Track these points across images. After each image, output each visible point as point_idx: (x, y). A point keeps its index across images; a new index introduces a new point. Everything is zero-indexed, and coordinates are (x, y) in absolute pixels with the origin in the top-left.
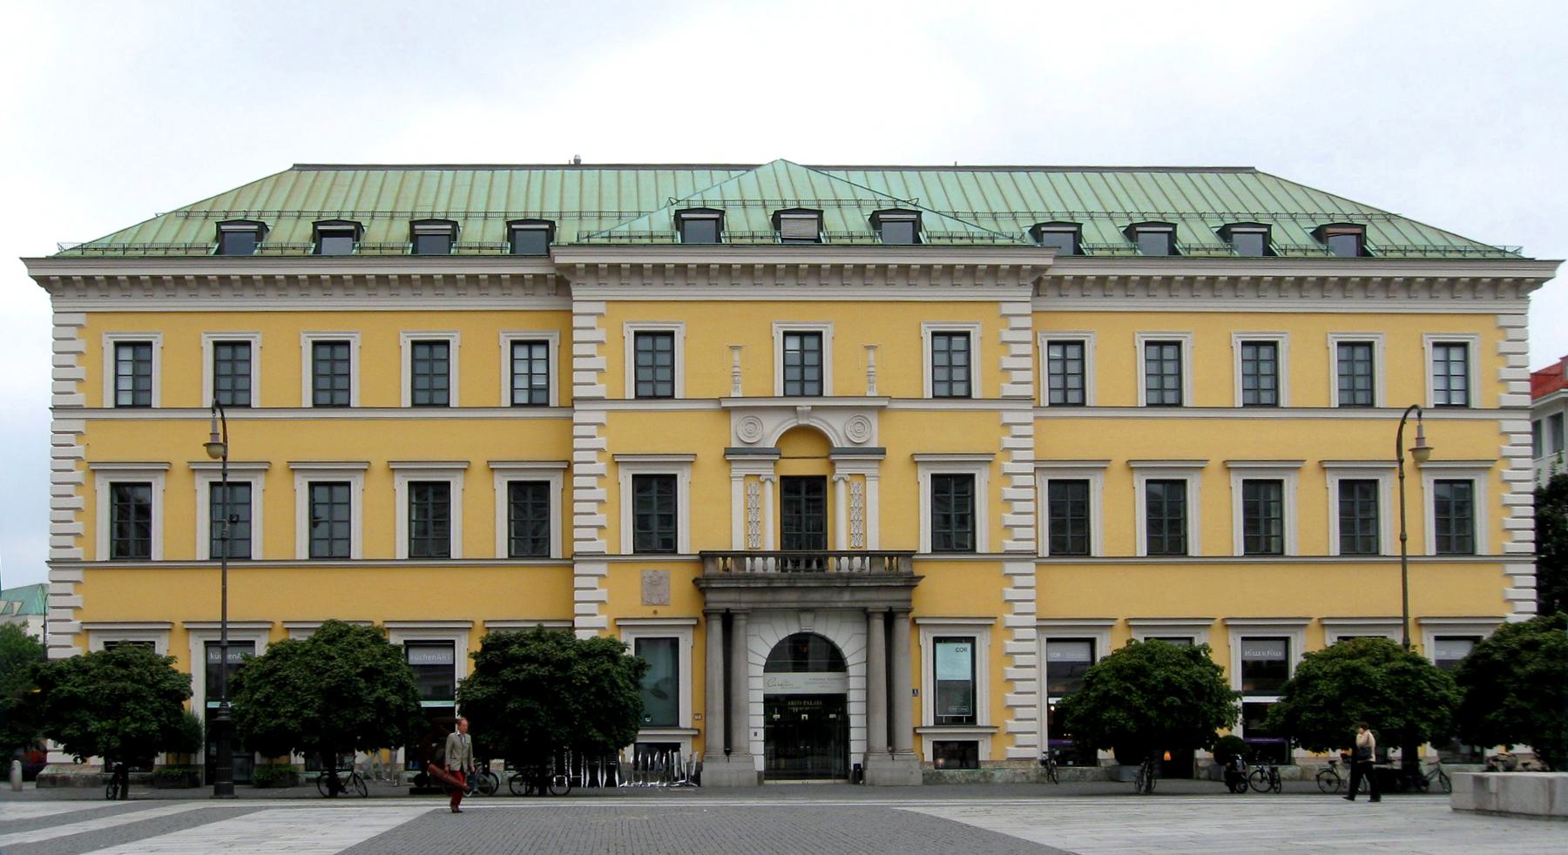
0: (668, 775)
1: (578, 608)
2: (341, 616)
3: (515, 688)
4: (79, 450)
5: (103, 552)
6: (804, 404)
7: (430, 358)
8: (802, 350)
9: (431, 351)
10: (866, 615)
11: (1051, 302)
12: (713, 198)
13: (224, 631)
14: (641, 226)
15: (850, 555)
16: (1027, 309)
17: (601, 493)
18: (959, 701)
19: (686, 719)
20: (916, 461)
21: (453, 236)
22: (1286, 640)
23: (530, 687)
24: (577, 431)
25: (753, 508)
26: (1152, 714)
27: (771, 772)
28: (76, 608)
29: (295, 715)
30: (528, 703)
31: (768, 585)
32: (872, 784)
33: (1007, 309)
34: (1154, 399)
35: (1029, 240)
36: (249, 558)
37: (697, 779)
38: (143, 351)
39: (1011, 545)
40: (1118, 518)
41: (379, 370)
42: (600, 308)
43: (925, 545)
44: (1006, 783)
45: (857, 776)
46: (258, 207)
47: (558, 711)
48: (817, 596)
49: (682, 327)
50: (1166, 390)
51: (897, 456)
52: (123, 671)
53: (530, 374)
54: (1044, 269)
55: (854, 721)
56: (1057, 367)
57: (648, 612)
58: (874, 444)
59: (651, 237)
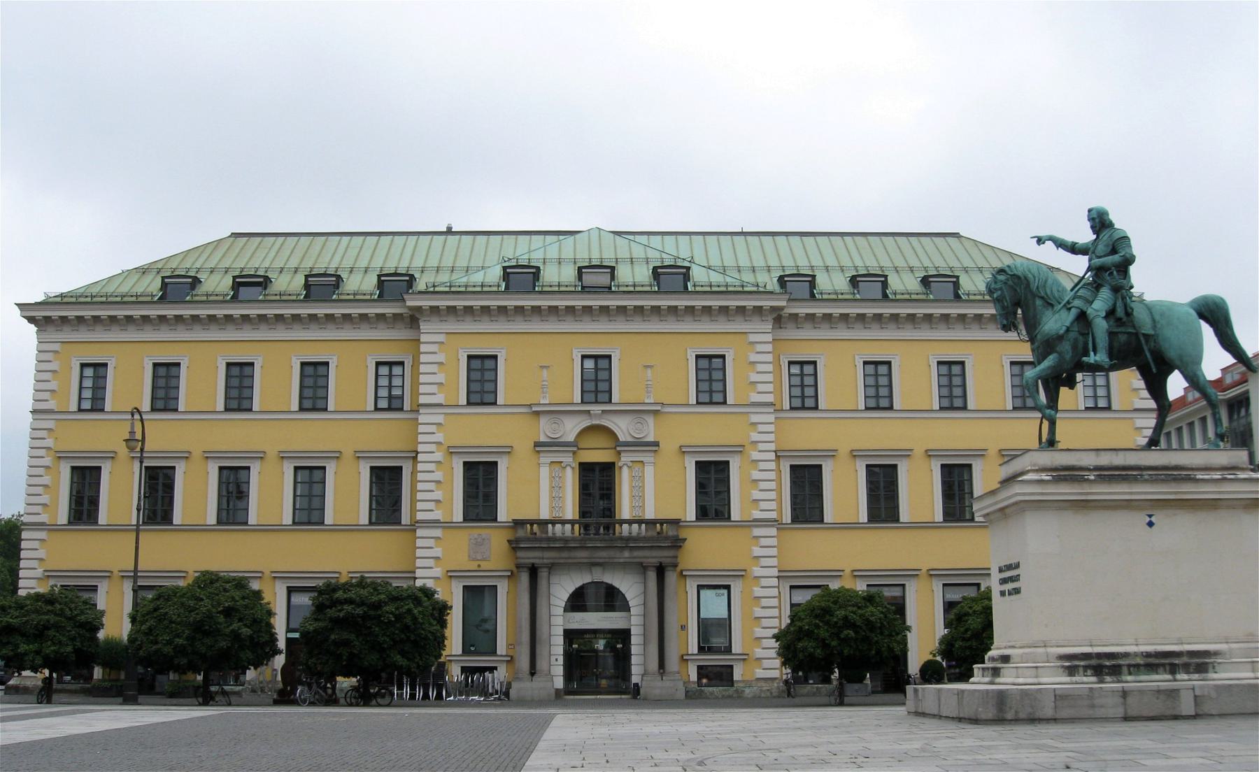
0: (484, 692)
1: (419, 563)
2: (213, 567)
3: (336, 622)
4: (49, 442)
5: (63, 518)
6: (596, 409)
7: (314, 377)
8: (596, 369)
9: (315, 369)
10: (642, 568)
11: (790, 333)
12: (536, 258)
13: (135, 578)
14: (477, 278)
15: (630, 522)
16: (769, 338)
17: (438, 476)
18: (713, 634)
19: (501, 648)
20: (683, 451)
21: (337, 286)
22: (903, 586)
23: (346, 623)
24: (421, 429)
25: (556, 487)
26: (834, 643)
27: (568, 691)
28: (41, 560)
29: (169, 642)
30: (345, 635)
31: (565, 545)
32: (645, 699)
33: (752, 338)
34: (946, 403)
35: (777, 288)
36: (246, 523)
37: (507, 694)
38: (101, 370)
39: (757, 514)
40: (845, 493)
41: (277, 384)
42: (441, 338)
43: (691, 514)
44: (754, 697)
45: (636, 691)
46: (334, 265)
47: (372, 644)
48: (604, 554)
49: (618, 352)
50: (880, 396)
51: (669, 447)
52: (50, 608)
53: (390, 387)
54: (782, 308)
55: (634, 650)
56: (796, 381)
57: (473, 565)
58: (651, 439)
59: (634, 286)
